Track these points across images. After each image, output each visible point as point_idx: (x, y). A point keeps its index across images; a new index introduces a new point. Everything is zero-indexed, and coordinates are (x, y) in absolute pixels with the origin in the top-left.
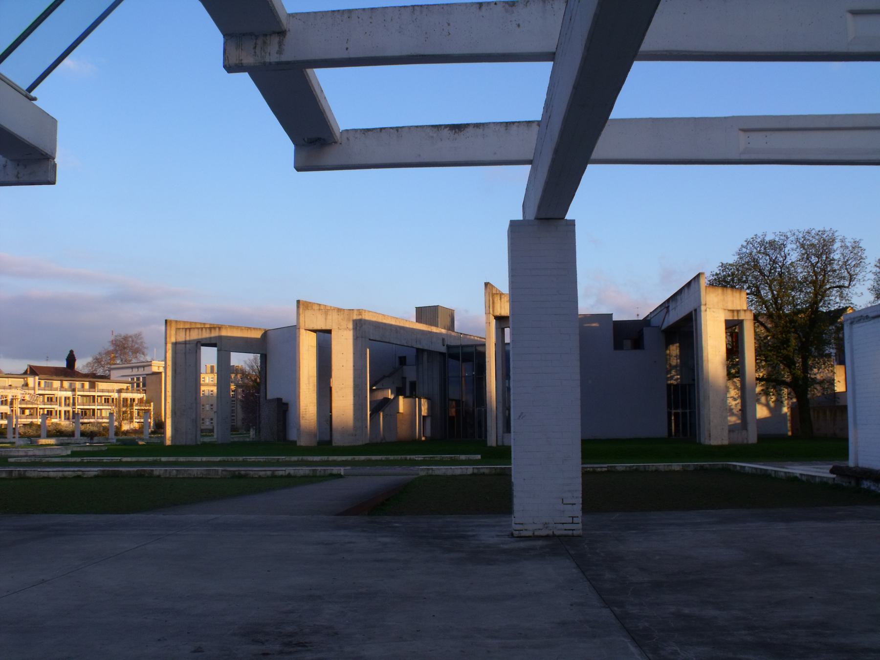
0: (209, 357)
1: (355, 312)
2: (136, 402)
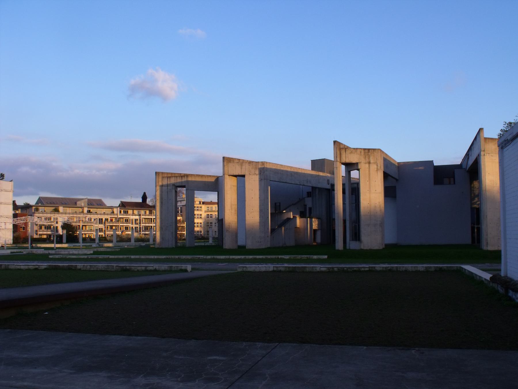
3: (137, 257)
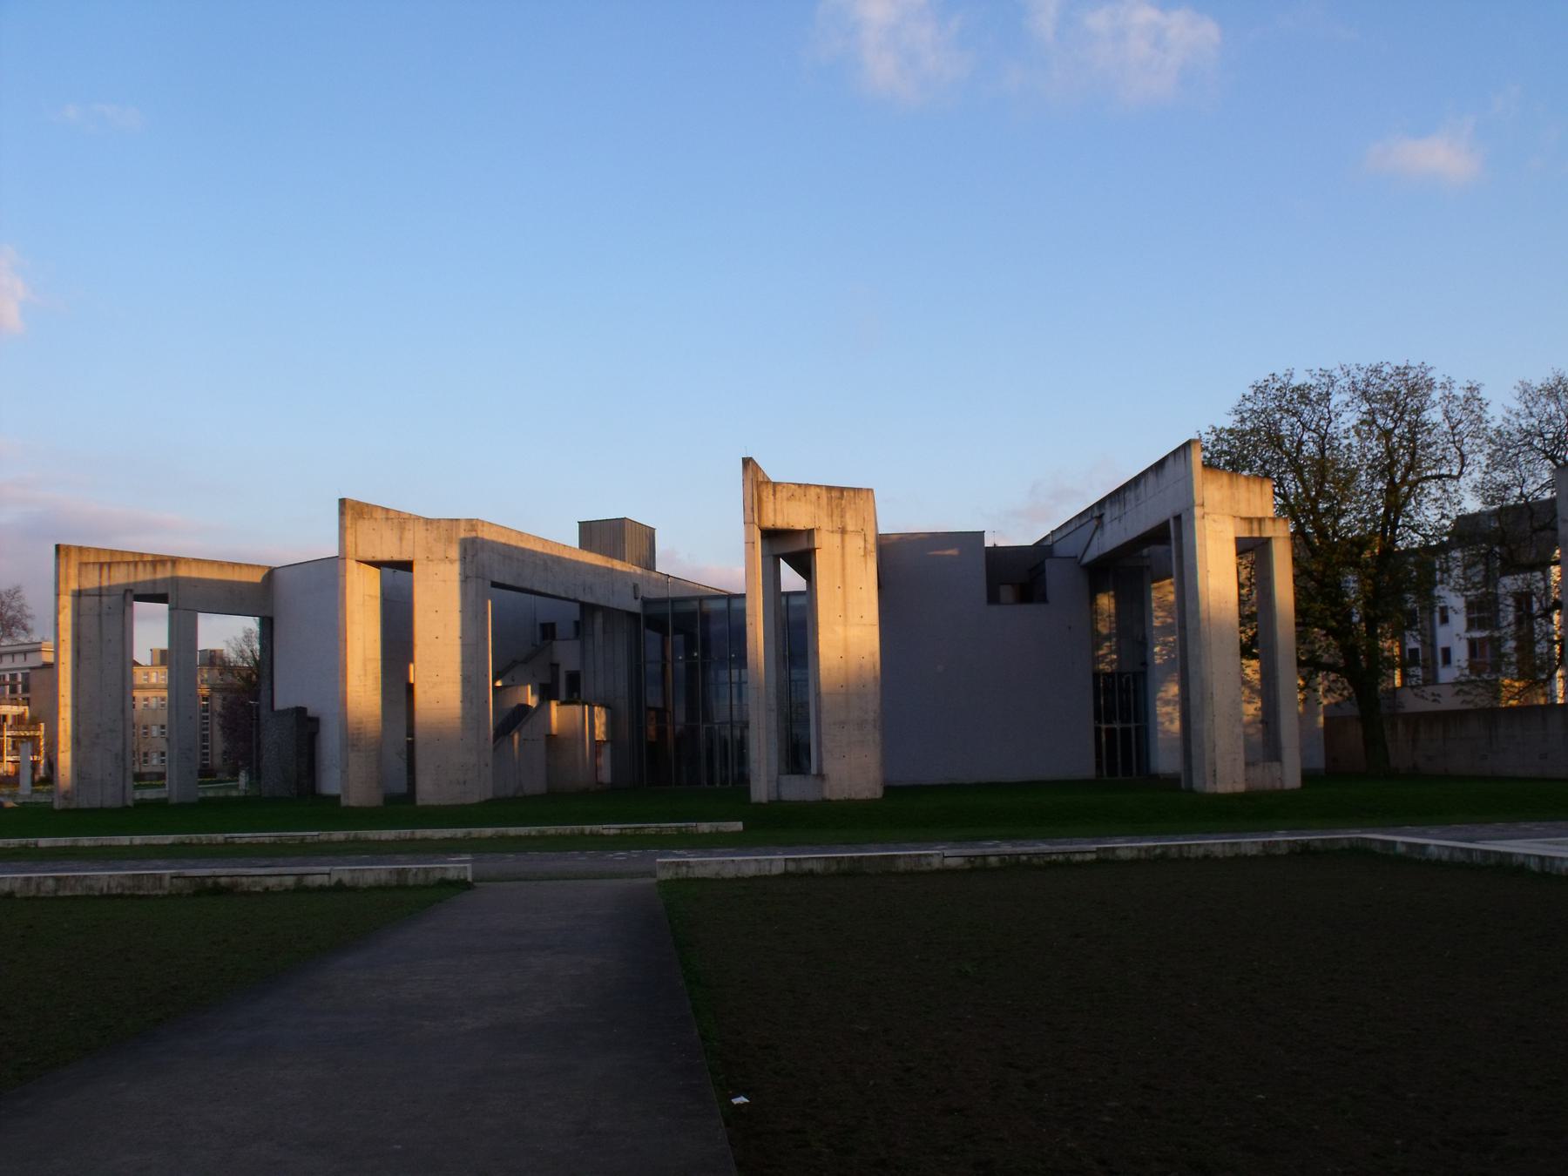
0: (150, 631)
1: (463, 525)
2: (10, 721)
3: (63, 841)
